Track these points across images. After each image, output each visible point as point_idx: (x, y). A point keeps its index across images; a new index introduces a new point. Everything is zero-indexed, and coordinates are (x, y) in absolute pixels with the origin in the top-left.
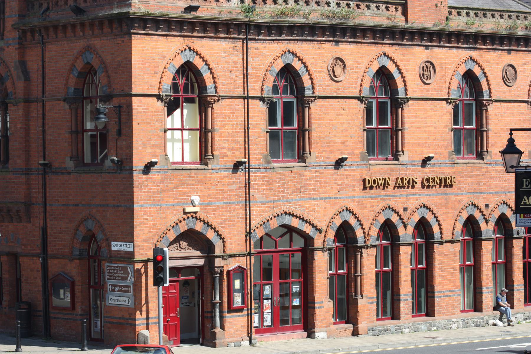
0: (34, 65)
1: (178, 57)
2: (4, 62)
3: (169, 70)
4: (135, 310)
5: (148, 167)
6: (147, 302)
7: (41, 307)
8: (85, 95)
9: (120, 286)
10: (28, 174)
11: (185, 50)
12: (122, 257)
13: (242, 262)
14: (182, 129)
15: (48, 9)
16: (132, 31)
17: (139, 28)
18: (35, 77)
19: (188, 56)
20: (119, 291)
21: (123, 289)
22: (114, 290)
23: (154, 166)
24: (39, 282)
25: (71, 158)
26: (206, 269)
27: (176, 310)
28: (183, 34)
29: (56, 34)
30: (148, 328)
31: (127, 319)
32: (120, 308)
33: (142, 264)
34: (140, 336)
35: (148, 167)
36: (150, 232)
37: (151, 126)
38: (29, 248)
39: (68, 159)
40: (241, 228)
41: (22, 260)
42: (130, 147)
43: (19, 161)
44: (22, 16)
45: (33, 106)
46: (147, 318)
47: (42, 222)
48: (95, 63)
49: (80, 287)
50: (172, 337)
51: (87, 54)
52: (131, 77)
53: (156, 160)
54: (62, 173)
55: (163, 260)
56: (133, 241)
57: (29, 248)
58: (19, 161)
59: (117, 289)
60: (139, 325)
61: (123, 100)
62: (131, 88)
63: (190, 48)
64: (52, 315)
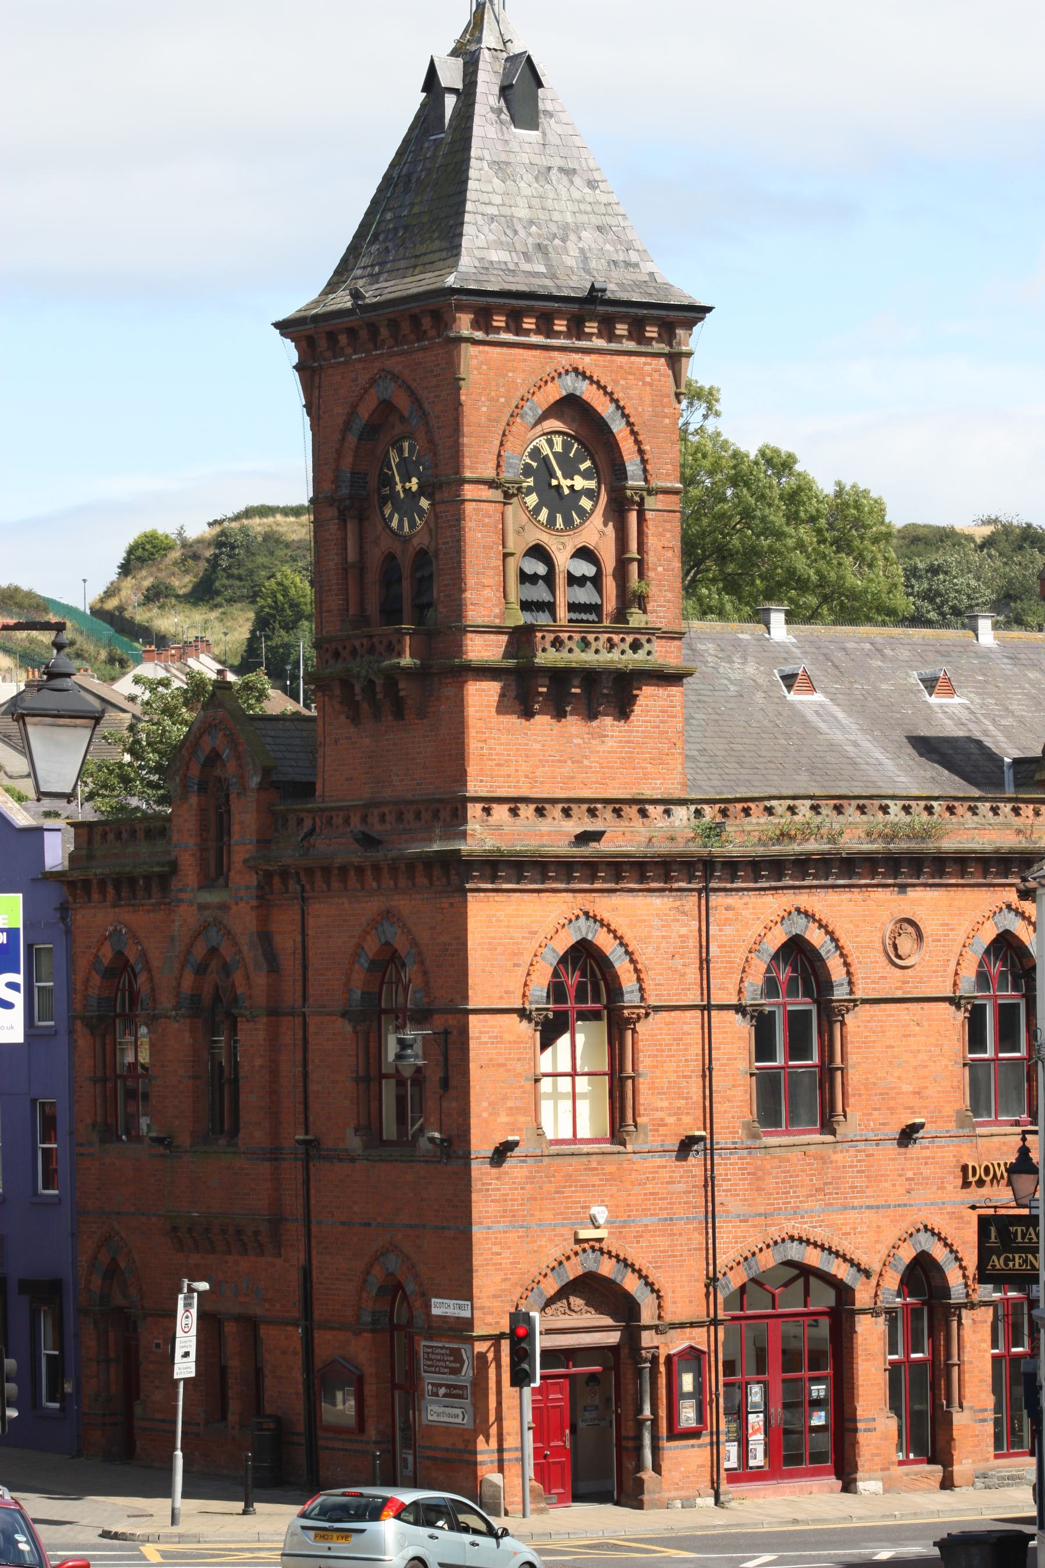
0: (286, 941)
1: (562, 933)
2: (229, 933)
3: (544, 959)
4: (475, 1434)
5: (502, 1152)
6: (499, 1419)
7: (300, 1427)
8: (383, 1006)
9: (448, 1386)
10: (276, 1159)
11: (578, 917)
13: (699, 1338)
14: (573, 1074)
16: (468, 886)
17: (482, 878)
18: (289, 965)
19: (583, 929)
21: (454, 1392)
22: (436, 1395)
23: (512, 1150)
25: (356, 1130)
26: (625, 1352)
27: (563, 1434)
30: (501, 1470)
32: (448, 1430)
33: (488, 1343)
34: (484, 1485)
35: (502, 1152)
36: (505, 1280)
37: (509, 1070)
39: (350, 1132)
40: (697, 1270)
41: (264, 1331)
42: (465, 1112)
44: (263, 843)
46: (501, 1450)
47: (302, 1256)
48: (401, 944)
53: (517, 1138)
54: (341, 1160)
55: (530, 1336)
56: (469, 1297)
57: (278, 1306)
59: (442, 1391)
60: (483, 1463)
61: (452, 1021)
62: (465, 998)
63: (586, 914)
64: (321, 1443)
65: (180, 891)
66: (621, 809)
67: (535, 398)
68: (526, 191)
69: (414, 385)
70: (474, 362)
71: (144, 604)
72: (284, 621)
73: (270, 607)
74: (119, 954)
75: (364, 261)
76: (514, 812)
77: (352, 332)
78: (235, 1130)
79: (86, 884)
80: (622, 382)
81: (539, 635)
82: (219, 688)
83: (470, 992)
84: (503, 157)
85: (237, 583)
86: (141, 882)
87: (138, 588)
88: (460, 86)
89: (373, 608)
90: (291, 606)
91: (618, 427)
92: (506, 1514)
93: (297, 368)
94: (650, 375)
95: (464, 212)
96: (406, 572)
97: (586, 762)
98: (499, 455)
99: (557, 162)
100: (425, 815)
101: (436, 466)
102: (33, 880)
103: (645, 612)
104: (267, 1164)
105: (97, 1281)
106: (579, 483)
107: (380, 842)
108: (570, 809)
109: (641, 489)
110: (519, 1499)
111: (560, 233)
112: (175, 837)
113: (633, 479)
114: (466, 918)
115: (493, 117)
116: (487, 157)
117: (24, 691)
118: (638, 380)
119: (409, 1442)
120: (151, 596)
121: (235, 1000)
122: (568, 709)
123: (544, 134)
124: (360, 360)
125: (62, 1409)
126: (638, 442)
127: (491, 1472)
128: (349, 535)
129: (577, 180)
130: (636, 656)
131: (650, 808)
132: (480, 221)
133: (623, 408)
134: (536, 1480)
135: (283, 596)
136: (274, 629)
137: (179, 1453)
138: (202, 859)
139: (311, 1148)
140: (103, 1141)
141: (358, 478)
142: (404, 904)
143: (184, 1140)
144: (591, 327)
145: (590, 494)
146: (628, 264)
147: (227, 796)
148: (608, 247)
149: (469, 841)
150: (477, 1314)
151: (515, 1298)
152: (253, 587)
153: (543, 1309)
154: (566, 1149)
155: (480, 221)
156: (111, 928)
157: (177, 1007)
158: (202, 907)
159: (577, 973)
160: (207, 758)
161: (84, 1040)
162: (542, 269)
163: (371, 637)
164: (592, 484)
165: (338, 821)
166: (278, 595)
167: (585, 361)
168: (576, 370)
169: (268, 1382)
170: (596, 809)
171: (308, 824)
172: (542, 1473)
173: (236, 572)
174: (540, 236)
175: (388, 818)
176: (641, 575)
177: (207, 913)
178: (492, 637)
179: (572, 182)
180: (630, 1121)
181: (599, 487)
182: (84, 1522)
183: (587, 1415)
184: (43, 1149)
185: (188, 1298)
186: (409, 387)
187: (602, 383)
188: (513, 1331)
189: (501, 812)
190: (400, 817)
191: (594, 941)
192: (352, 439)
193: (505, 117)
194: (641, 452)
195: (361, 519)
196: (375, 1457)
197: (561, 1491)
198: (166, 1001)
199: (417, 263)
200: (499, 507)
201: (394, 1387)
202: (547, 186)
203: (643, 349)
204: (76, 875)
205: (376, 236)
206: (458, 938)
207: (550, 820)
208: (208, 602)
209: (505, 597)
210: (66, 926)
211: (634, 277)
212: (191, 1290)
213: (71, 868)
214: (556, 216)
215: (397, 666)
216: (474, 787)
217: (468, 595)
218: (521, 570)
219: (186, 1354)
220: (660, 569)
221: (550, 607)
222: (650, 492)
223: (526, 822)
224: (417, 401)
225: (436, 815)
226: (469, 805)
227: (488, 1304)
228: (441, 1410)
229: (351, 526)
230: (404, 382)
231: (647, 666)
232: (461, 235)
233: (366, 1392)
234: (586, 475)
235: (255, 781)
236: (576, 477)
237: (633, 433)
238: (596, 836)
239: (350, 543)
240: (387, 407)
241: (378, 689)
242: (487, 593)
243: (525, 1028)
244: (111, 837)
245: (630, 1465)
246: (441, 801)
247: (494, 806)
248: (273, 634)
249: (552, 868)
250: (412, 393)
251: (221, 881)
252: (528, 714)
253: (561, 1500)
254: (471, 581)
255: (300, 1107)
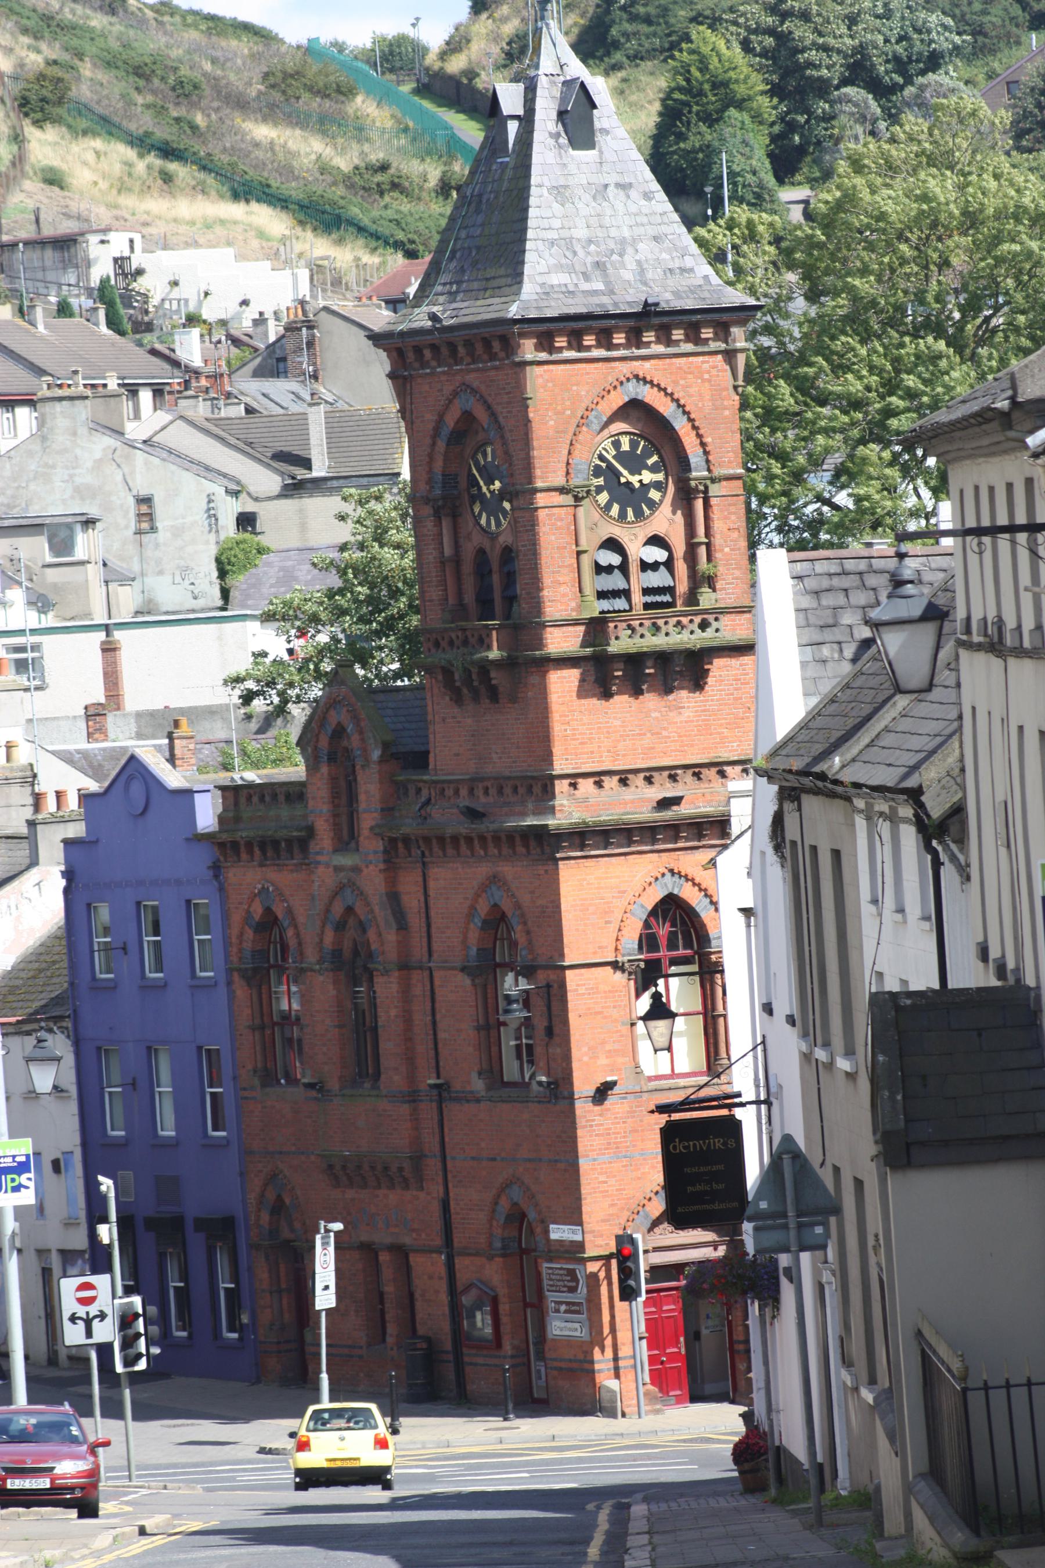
0: (412, 901)
1: (649, 890)
2: (362, 893)
3: (633, 914)
4: (592, 1344)
5: (603, 1092)
6: (613, 1330)
7: (448, 1346)
8: (498, 960)
9: (567, 1303)
10: (414, 1101)
11: (663, 875)
12: (567, 1252)
15: (429, 800)
16: (558, 855)
17: (571, 847)
18: (416, 922)
19: (670, 885)
20: (566, 1312)
21: (573, 1308)
22: (557, 1311)
23: (612, 1089)
24: (444, 1298)
25: (480, 1074)
27: (678, 1342)
28: (657, 847)
29: (444, 850)
30: (617, 1376)
31: (580, 1361)
32: (569, 1342)
33: (599, 1263)
34: (602, 1391)
35: (603, 1092)
36: (612, 1205)
37: (605, 1017)
38: (423, 1236)
39: (474, 1076)
41: (415, 1260)
42: (567, 1057)
43: (396, 1078)
44: (387, 811)
45: (416, 976)
46: (616, 1359)
47: (441, 1189)
48: (506, 906)
49: (507, 1307)
50: (673, 1389)
51: (494, 888)
52: (561, 935)
53: (615, 1078)
54: (468, 1101)
55: (634, 1256)
56: (580, 1223)
57: (423, 1236)
58: (396, 1078)
59: (563, 1308)
60: (600, 1371)
61: (552, 976)
62: (562, 956)
63: (671, 871)
64: (466, 1359)
65: (318, 853)
66: (700, 773)
67: (599, 407)
68: (584, 211)
69: (490, 400)
70: (540, 381)
71: (505, 66)
72: (705, 111)
73: (680, 89)
74: (268, 911)
75: (444, 278)
76: (599, 784)
77: (434, 348)
78: (377, 1075)
79: (235, 845)
80: (682, 382)
81: (611, 625)
82: (341, 666)
83: (566, 951)
84: (562, 182)
85: (645, 29)
86: (283, 844)
87: (496, 38)
88: (520, 112)
89: (469, 598)
90: (715, 86)
91: (680, 425)
92: (624, 1415)
93: (209, 868)
94: (708, 372)
95: (525, 240)
96: (495, 566)
97: (665, 733)
98: (568, 464)
99: (612, 179)
100: (521, 790)
101: (512, 475)
102: (187, 840)
103: (714, 590)
104: (406, 1106)
105: (265, 1217)
106: (647, 477)
107: (483, 815)
108: (651, 777)
109: (705, 479)
110: (635, 1402)
111: (616, 248)
112: (311, 803)
113: (697, 470)
114: (559, 884)
115: (552, 142)
116: (547, 183)
117: (283, 336)
118: (696, 377)
119: (541, 1356)
120: (515, 52)
121: (370, 955)
122: (644, 687)
123: (601, 152)
124: (444, 373)
125: (240, 1339)
126: (699, 436)
127: (609, 1378)
128: (445, 531)
129: (633, 193)
130: (704, 634)
131: (728, 769)
132: (541, 247)
133: (684, 406)
134: (653, 1383)
135: (701, 70)
136: (689, 123)
137: (324, 1377)
138: (335, 824)
139: (442, 1091)
140: (264, 1085)
141: (449, 480)
142: (508, 870)
143: (333, 1085)
144: (649, 336)
145: (658, 486)
146: (683, 270)
147: (354, 766)
148: (665, 256)
149: (558, 815)
150: (588, 1238)
151: (623, 1221)
152: (669, 35)
153: (651, 1230)
154: (664, 1083)
155: (541, 247)
156: (259, 886)
157: (321, 961)
158: (338, 869)
159: (667, 924)
160: (334, 731)
161: (241, 991)
162: (600, 286)
163: (464, 630)
164: (660, 477)
165: (449, 792)
166: (693, 69)
167: (645, 368)
168: (637, 377)
169: (419, 1305)
170: (676, 775)
171: (425, 793)
172: (660, 1378)
173: (642, 10)
174: (598, 253)
175: (490, 791)
176: (710, 558)
177: (342, 874)
178: (570, 628)
179: (628, 197)
180: (723, 1055)
181: (667, 479)
182: (246, 1442)
183: (710, 1323)
184: (212, 1094)
185: (325, 1238)
186: (485, 402)
187: (663, 386)
188: (619, 1251)
189: (586, 786)
190: (500, 790)
191: (681, 895)
192: (441, 445)
193: (564, 140)
194: (703, 444)
195: (455, 516)
196: (506, 1371)
197: (678, 1392)
198: (311, 956)
199: (488, 287)
200: (571, 510)
201: (526, 1305)
202: (605, 204)
203: (700, 349)
204: (224, 837)
205: (454, 252)
206: (553, 902)
207: (632, 789)
208: (602, 60)
209: (580, 591)
210: (220, 883)
211: (689, 282)
212: (327, 1231)
213: (221, 831)
214: (613, 232)
215: (486, 660)
216: (560, 766)
217: (545, 593)
218: (597, 564)
219: (326, 1288)
220: (727, 550)
221: (626, 594)
222: (713, 480)
223: (610, 793)
224: (493, 415)
225: (530, 790)
226: (557, 782)
227: (597, 1228)
228: (563, 1324)
229: (446, 524)
230: (482, 397)
231: (715, 644)
232: (523, 263)
233: (501, 1311)
234: (654, 469)
235: (376, 754)
236: (644, 472)
237: (695, 428)
238: (677, 801)
239: (446, 540)
240: (468, 417)
241: (474, 677)
242: (563, 589)
243: (619, 978)
244: (255, 799)
245: (741, 1366)
246: (533, 778)
247: (580, 780)
248: (688, 130)
249: (636, 833)
250: (489, 407)
251: (353, 845)
252: (607, 695)
253: (679, 1401)
254: (547, 579)
255: (432, 1053)
